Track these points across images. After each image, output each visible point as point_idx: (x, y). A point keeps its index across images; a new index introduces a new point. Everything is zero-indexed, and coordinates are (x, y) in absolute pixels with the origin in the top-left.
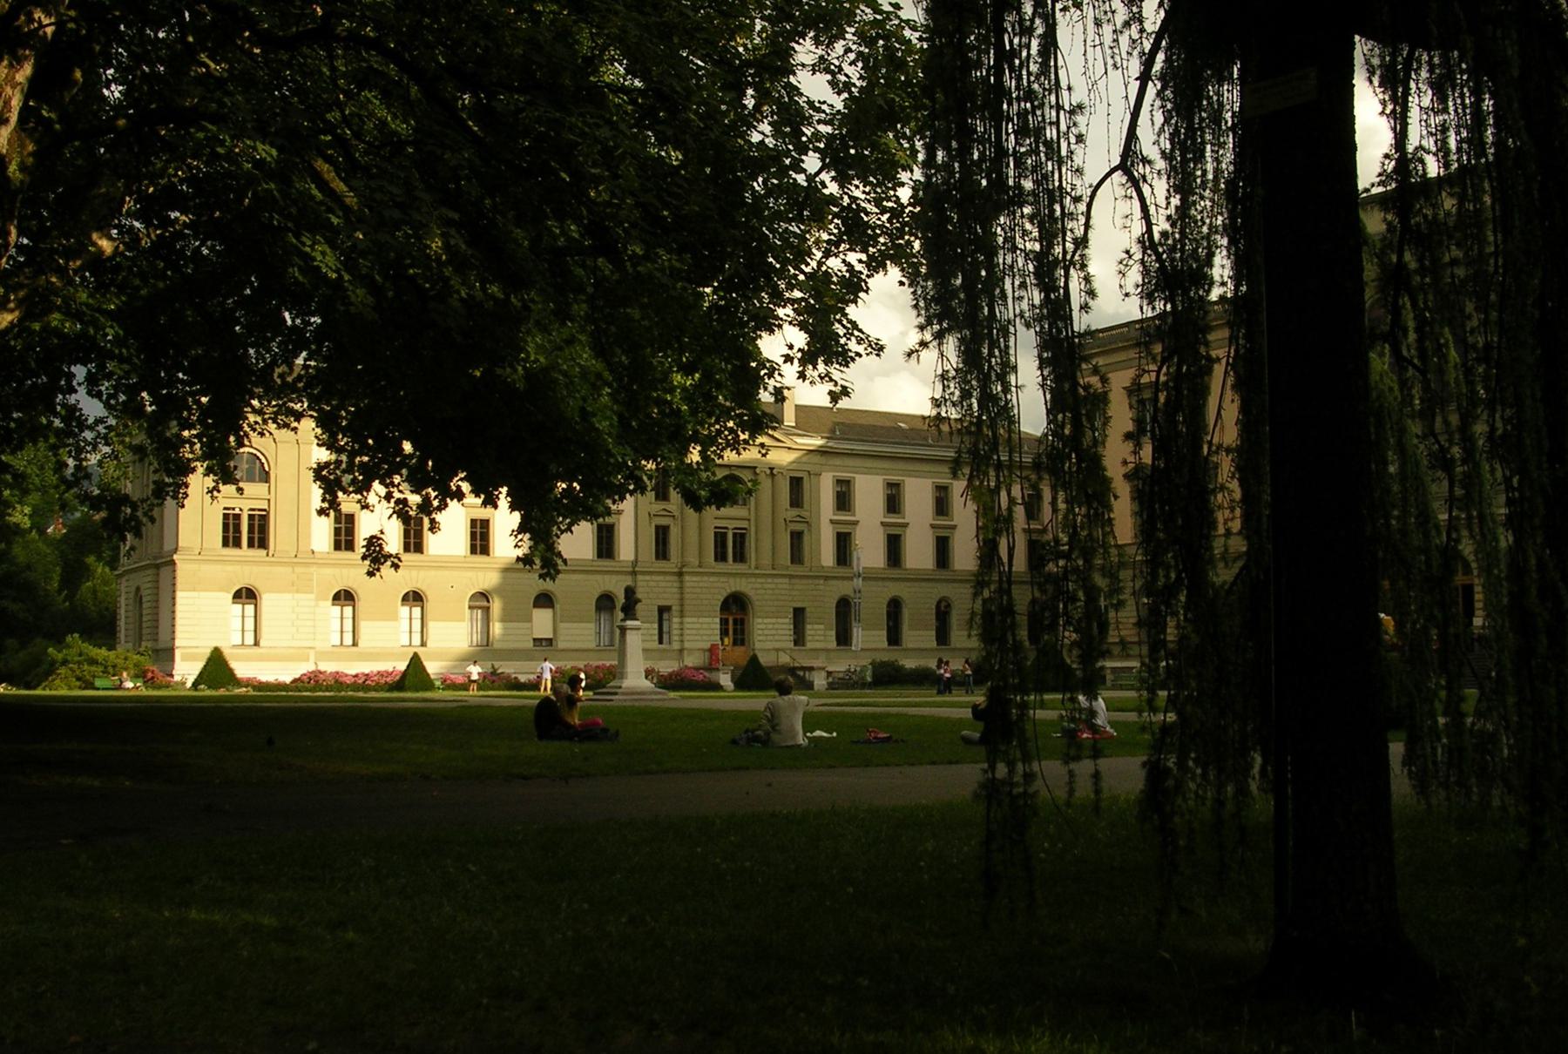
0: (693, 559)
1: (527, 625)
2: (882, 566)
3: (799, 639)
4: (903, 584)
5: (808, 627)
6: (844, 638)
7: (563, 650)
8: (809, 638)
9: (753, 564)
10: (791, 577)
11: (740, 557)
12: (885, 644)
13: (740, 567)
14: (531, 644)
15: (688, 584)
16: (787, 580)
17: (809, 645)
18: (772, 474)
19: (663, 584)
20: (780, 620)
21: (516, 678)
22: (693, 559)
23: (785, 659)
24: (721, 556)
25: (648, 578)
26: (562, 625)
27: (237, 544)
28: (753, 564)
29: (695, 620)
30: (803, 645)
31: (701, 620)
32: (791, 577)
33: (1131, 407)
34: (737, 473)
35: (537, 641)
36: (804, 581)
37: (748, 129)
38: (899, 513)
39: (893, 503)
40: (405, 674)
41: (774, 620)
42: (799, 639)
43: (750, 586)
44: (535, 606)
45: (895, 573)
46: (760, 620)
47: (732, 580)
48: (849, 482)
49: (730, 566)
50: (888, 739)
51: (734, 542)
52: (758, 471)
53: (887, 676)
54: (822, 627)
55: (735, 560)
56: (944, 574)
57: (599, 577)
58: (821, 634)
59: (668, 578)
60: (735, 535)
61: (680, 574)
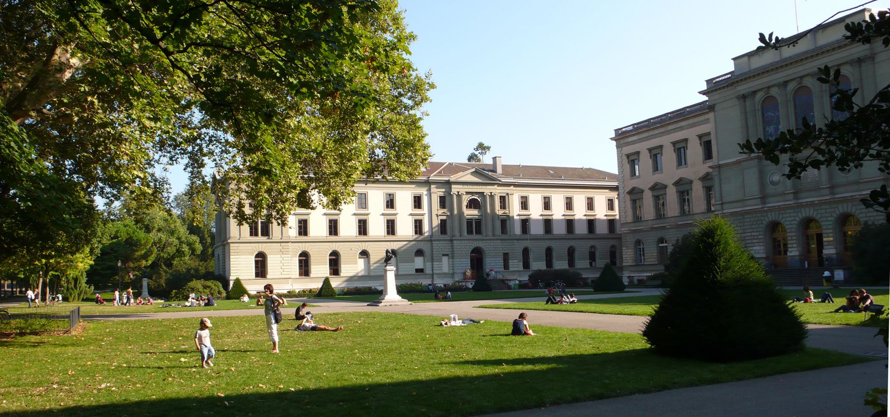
0: (457, 233)
1: (412, 264)
2: (542, 233)
3: (506, 266)
4: (552, 241)
5: (510, 261)
6: (526, 265)
7: (401, 275)
8: (511, 266)
9: (484, 235)
10: (502, 240)
11: (479, 232)
12: (522, 269)
13: (265, 239)
14: (414, 272)
15: (455, 245)
16: (500, 241)
17: (511, 269)
18: (458, 194)
19: (445, 245)
20: (497, 259)
21: (375, 288)
22: (457, 233)
23: (500, 277)
24: (470, 232)
25: (437, 242)
26: (400, 264)
27: (256, 235)
28: (484, 235)
29: (459, 260)
30: (508, 269)
31: (462, 260)
32: (502, 240)
33: (426, 147)
34: (687, 203)
35: (417, 270)
36: (508, 241)
37: (203, 10)
38: (593, 210)
39: (390, 204)
40: (321, 289)
41: (494, 259)
42: (506, 266)
43: (483, 244)
44: (415, 256)
45: (591, 236)
46: (488, 259)
47: (475, 242)
48: (571, 198)
49: (475, 236)
50: (314, 329)
51: (476, 226)
52: (485, 194)
53: (325, 293)
54: (516, 261)
55: (262, 235)
56: (571, 236)
57: (300, 244)
58: (516, 264)
59: (446, 242)
60: (476, 222)
61: (451, 240)
